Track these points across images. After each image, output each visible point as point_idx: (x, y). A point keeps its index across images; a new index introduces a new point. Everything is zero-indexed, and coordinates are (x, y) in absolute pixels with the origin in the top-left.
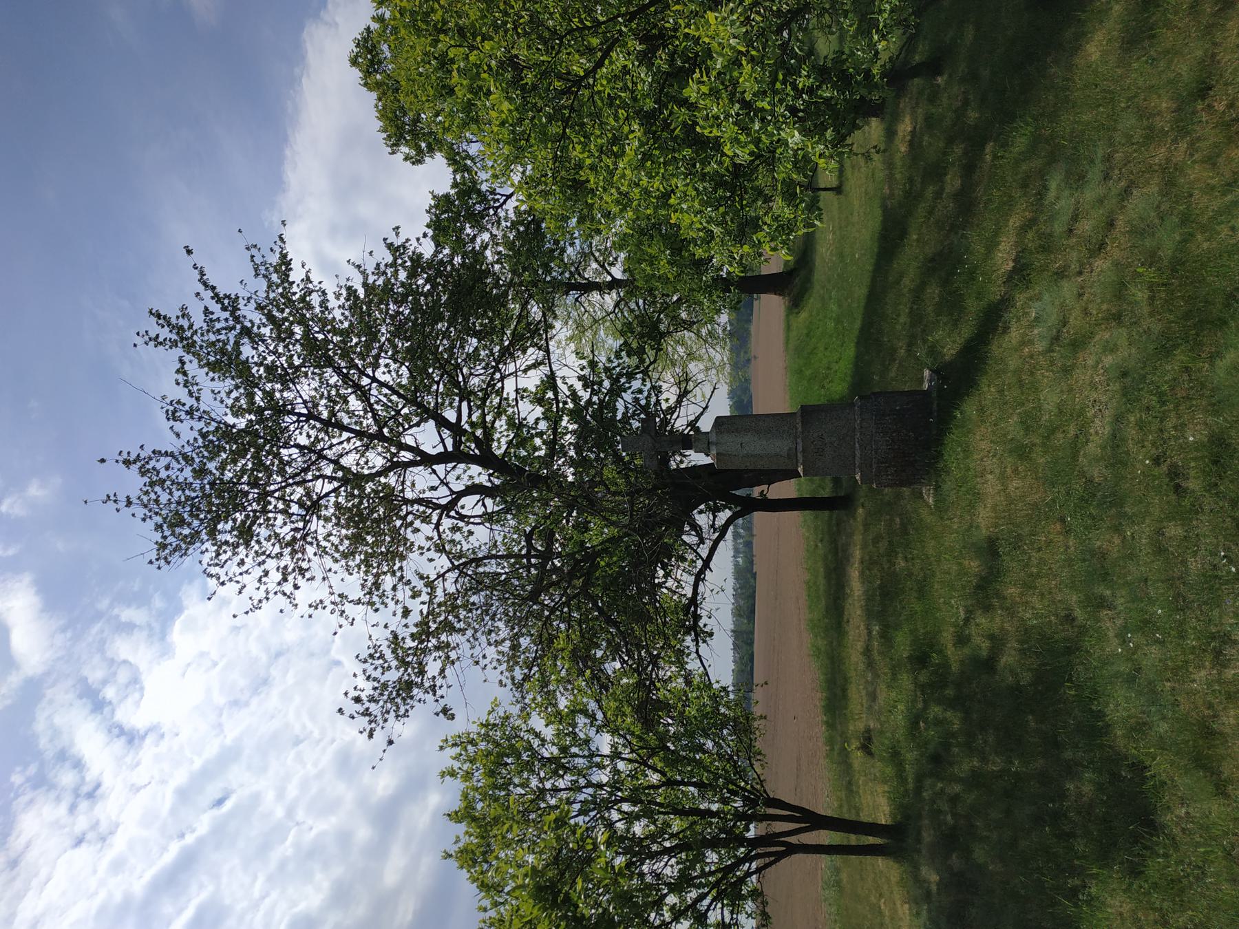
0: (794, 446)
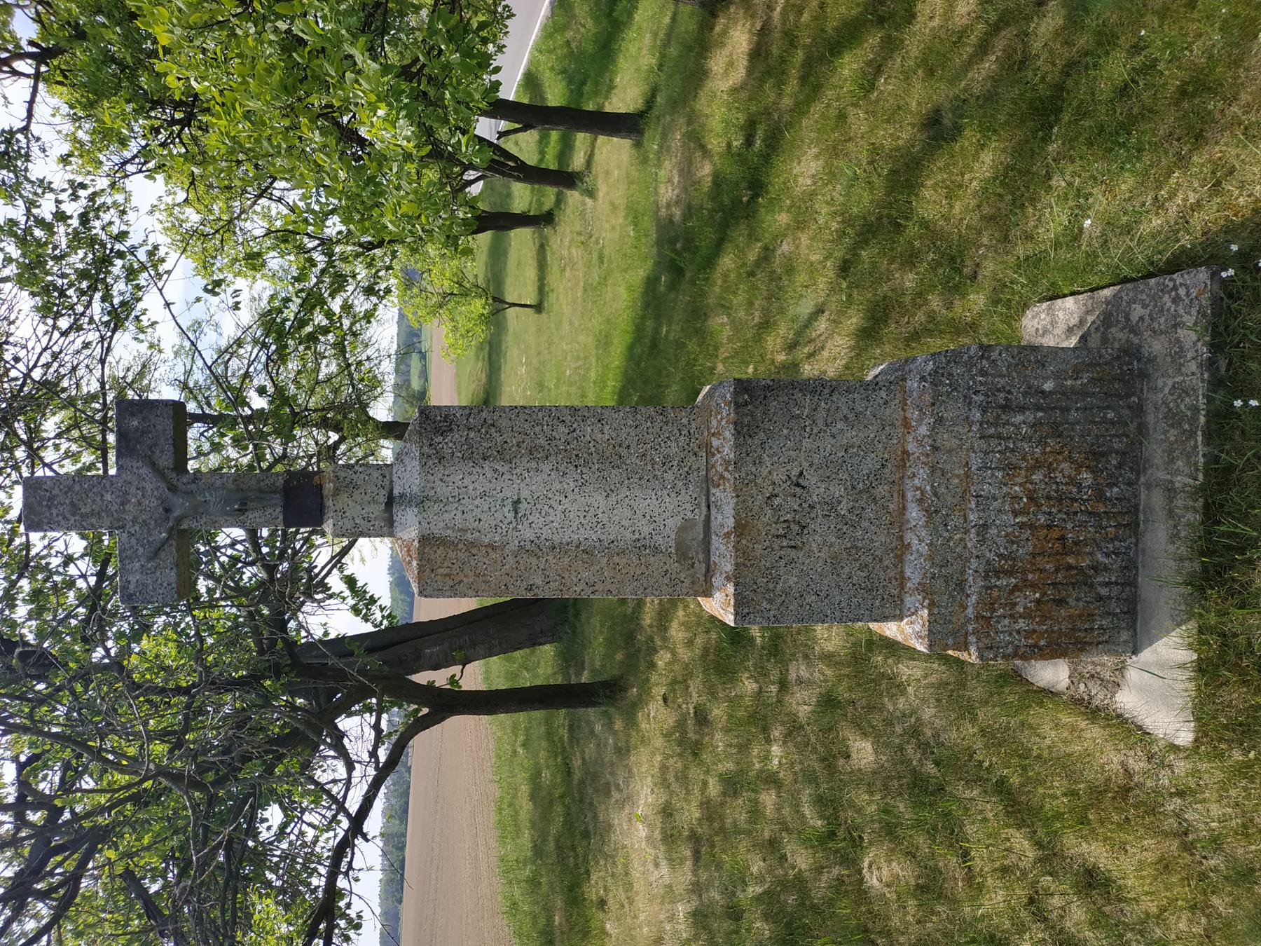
0: (700, 517)
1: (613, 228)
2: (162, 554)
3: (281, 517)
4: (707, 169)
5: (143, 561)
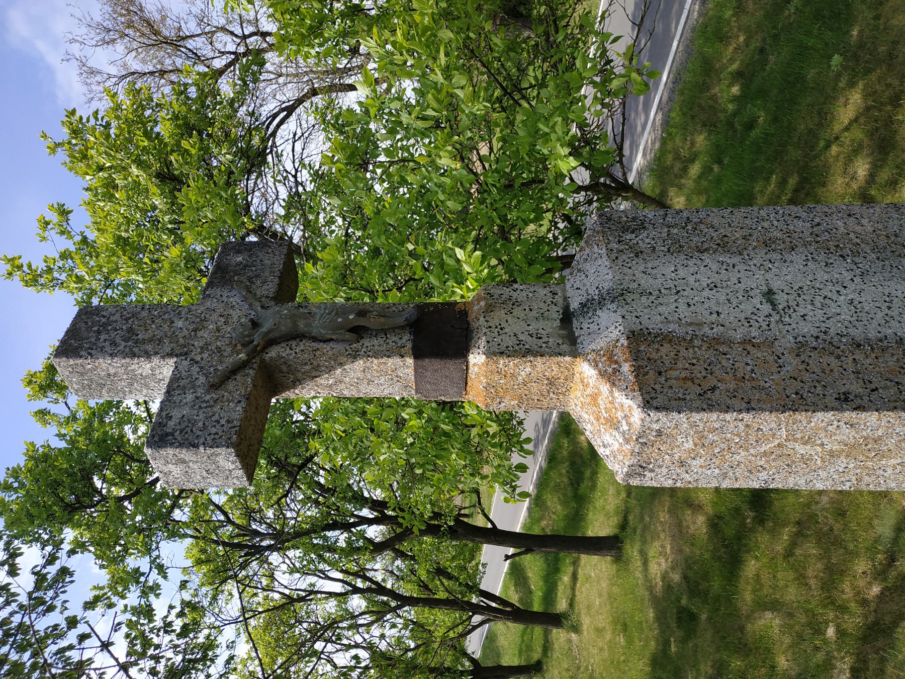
1: (601, 649)
2: (231, 385)
3: (409, 345)
4: (701, 519)
5: (200, 392)
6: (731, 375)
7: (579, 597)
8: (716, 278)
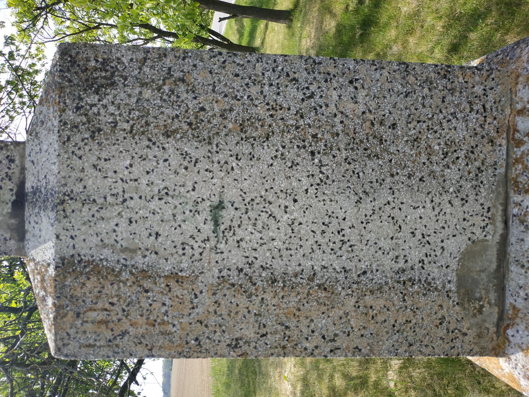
4: (333, 24)
6: (145, 317)
7: (267, 40)
8: (171, 181)
